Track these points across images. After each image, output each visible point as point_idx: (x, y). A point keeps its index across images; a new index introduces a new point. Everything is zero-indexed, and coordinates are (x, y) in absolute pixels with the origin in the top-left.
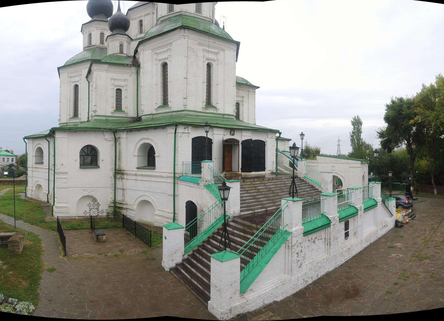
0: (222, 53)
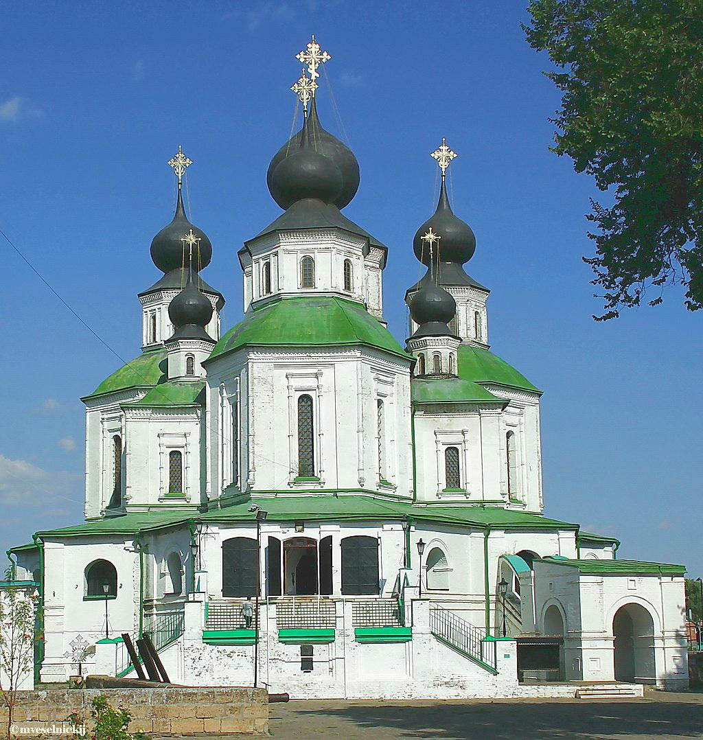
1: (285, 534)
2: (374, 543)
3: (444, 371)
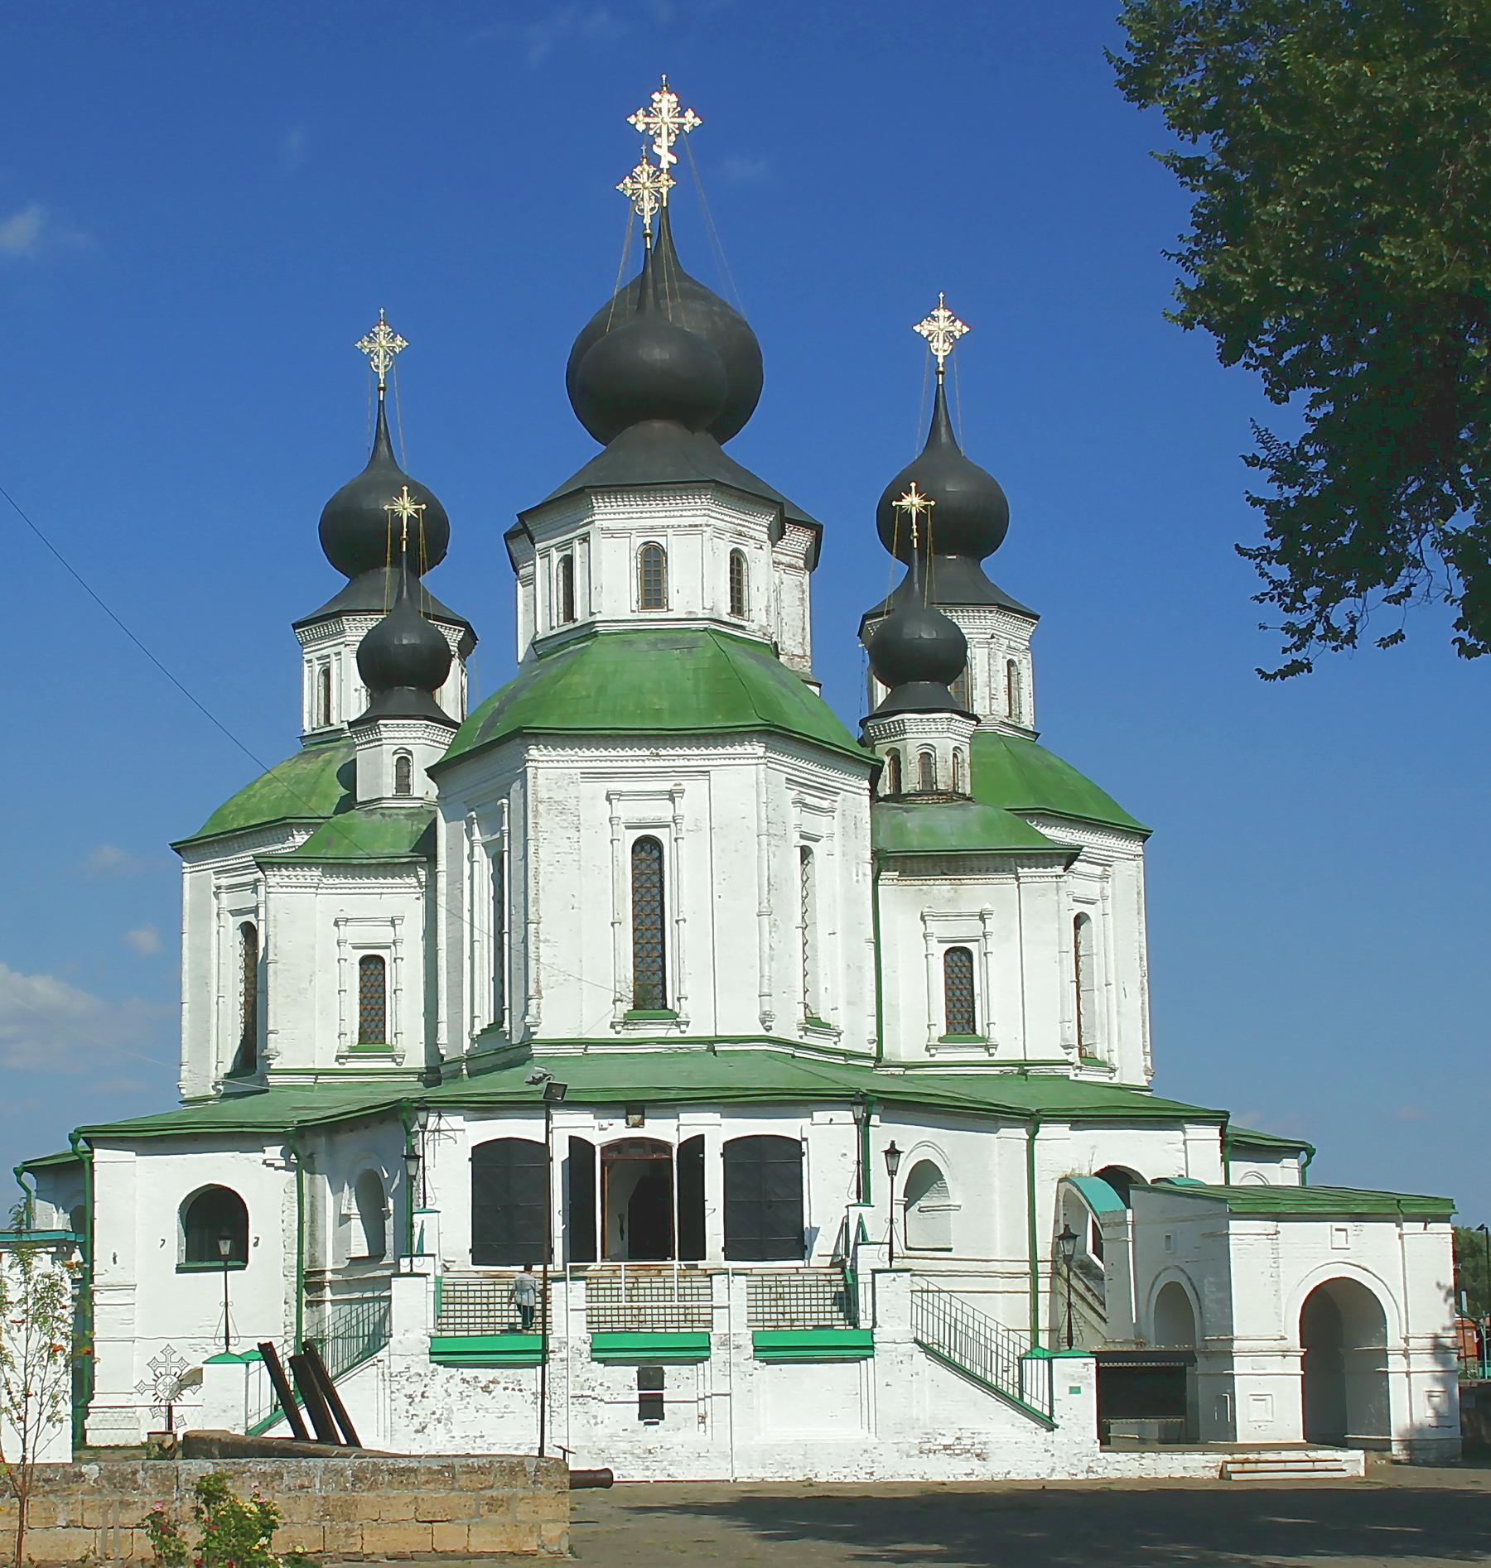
0: (694, 788)
1: (603, 1131)
2: (792, 1150)
3: (941, 787)
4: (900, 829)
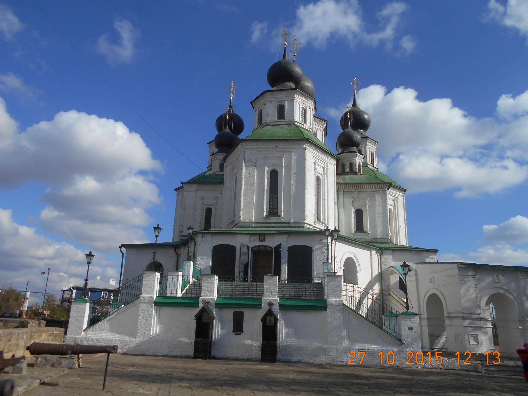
4: (345, 179)
